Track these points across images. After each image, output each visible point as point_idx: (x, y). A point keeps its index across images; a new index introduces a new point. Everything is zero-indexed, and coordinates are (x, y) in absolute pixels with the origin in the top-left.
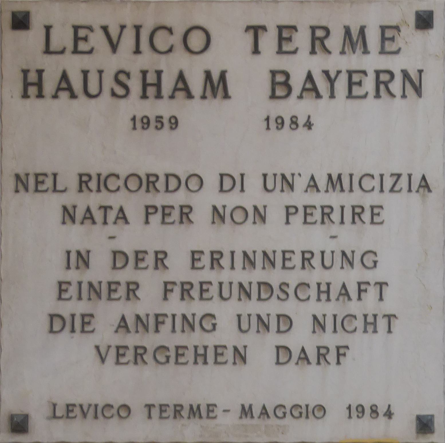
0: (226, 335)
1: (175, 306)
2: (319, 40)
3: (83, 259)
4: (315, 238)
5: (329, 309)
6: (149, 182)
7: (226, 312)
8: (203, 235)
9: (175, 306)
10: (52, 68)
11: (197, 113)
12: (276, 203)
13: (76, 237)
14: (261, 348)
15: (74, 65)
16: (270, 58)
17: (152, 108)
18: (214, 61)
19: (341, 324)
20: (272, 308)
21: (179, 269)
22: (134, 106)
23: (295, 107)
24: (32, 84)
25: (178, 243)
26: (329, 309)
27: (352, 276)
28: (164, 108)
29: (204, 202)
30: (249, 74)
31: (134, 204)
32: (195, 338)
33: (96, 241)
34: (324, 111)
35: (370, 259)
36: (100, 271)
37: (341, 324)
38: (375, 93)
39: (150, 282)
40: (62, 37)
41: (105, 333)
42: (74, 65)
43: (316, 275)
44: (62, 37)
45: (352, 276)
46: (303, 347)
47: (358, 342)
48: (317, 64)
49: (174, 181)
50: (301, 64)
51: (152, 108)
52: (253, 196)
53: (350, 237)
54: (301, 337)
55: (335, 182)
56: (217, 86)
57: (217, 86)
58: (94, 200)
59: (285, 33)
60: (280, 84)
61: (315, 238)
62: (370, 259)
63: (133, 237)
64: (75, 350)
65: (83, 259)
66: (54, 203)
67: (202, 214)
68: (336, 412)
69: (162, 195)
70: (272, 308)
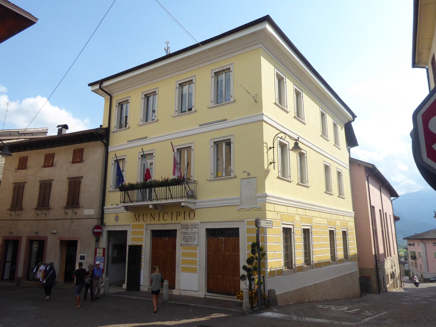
8: (189, 235)
63: (186, 235)
69: (187, 233)
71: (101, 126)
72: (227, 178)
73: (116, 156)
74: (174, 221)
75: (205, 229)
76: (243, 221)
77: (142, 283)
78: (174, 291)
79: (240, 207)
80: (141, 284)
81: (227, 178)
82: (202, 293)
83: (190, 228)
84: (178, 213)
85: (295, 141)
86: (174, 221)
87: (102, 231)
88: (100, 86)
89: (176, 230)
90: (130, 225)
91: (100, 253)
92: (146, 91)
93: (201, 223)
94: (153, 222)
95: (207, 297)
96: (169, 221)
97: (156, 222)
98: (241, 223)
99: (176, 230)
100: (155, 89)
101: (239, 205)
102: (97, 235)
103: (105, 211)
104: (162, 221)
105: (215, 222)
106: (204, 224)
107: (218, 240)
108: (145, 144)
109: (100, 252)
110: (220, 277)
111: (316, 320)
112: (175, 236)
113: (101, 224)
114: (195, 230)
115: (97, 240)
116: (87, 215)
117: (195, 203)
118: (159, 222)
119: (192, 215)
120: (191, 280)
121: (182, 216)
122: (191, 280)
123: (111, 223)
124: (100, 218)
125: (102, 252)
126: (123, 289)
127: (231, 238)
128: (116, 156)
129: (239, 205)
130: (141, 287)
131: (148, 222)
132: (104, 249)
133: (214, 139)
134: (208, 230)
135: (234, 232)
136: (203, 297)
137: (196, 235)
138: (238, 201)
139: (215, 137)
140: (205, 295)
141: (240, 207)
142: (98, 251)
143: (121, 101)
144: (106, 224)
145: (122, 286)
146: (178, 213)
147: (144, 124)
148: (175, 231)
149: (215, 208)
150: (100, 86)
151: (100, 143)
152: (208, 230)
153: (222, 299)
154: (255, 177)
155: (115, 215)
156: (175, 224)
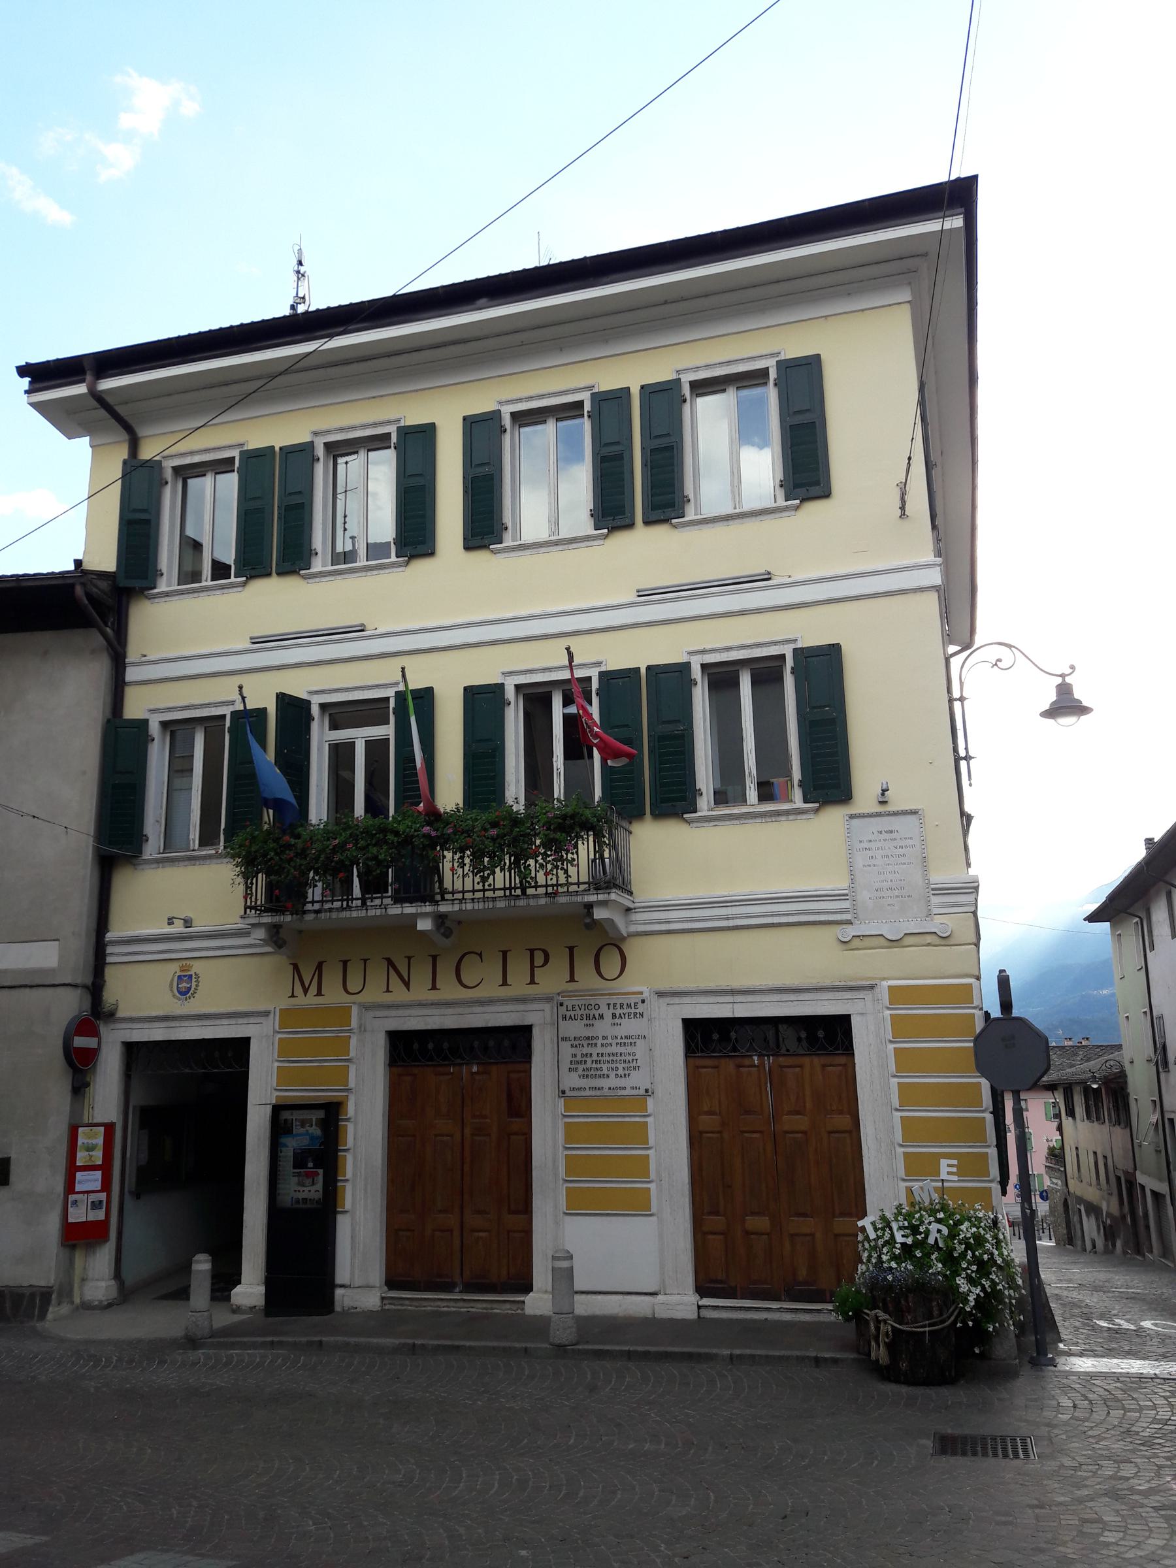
0: (605, 1072)
1: (594, 1065)
2: (622, 1006)
3: (575, 1056)
4: (622, 1050)
5: (626, 1065)
6: (588, 1038)
7: (605, 1067)
8: (599, 1050)
9: (594, 1065)
10: (568, 1014)
11: (597, 1023)
12: (614, 1042)
13: (574, 1051)
14: (612, 1074)
15: (572, 1013)
16: (612, 1011)
17: (588, 1022)
18: (600, 1011)
19: (629, 1068)
20: (614, 1065)
21: (595, 1057)
22: (585, 1022)
23: (616, 1021)
24: (564, 1018)
25: (594, 1051)
26: (626, 1065)
27: (631, 1058)
28: (591, 1022)
29: (599, 1042)
30: (608, 1014)
31: (585, 1043)
32: (599, 1072)
33: (578, 1051)
34: (624, 1021)
35: (634, 1054)
36: (579, 1058)
37: (629, 1068)
38: (378, 1239)
39: (589, 1060)
40: (570, 1008)
41: (580, 1072)
42: (572, 1013)
43: (623, 1058)
44: (570, 1008)
45: (631, 1058)
46: (41, 375)
47: (632, 1072)
48: (621, 1011)
49: (593, 1038)
50: (618, 1012)
51: (588, 1022)
52: (609, 1041)
53: (630, 1049)
54: (620, 1072)
55: (626, 1037)
56: (601, 1017)
57: (601, 1017)
58: (577, 1042)
59: (615, 1005)
60: (614, 1016)
61: (622, 1050)
62: (634, 1054)
63: (585, 1050)
64: (575, 1075)
65: (575, 1056)
66: (569, 1043)
67: (599, 1045)
68: (628, 1088)
69: (591, 1041)
70: (614, 1065)
71: (78, 563)
72: (205, 857)
73: (404, 676)
74: (519, 985)
75: (680, 1024)
76: (872, 987)
77: (342, 1274)
78: (529, 1299)
79: (851, 931)
80: (339, 1280)
81: (205, 857)
82: (681, 1301)
83: (608, 1014)
84: (539, 959)
85: (1059, 680)
86: (519, 985)
87: (99, 1043)
88: (79, 387)
89: (528, 1029)
90: (266, 1014)
91: (90, 1148)
92: (336, 430)
93: (661, 994)
94: (399, 993)
95: (706, 1314)
96: (491, 988)
97: (420, 991)
98: (861, 995)
99: (528, 1029)
100: (383, 423)
101: (849, 922)
102: (80, 1064)
103: (109, 950)
104: (449, 990)
105: (733, 992)
106: (676, 1000)
107: (739, 1066)
108: (347, 655)
109: (91, 1141)
110: (760, 1223)
111: (482, 1343)
112: (525, 1054)
113: (96, 1013)
114: (629, 1027)
115: (80, 1088)
116: (13, 971)
117: (628, 910)
118: (433, 996)
119: (610, 964)
120: (620, 1249)
121: (559, 964)
122: (620, 1249)
123: (146, 1001)
124: (89, 981)
125: (100, 1141)
126: (237, 1310)
127: (807, 1060)
128: (404, 676)
129: (849, 922)
130: (339, 1292)
131: (374, 993)
132: (109, 1128)
133: (704, 652)
134: (691, 1026)
135: (506, 1043)
136: (691, 1314)
137: (640, 1049)
138: (845, 905)
139: (708, 647)
140: (699, 1307)
141: (851, 931)
142: (83, 1137)
143: (188, 460)
144: (121, 1014)
145: (228, 1298)
146: (539, 959)
147: (787, 508)
148: (525, 1031)
149: (163, 964)
150: (79, 387)
151: (95, 639)
152: (691, 1026)
153: (788, 1317)
154: (914, 812)
155: (174, 968)
156: (524, 1000)
